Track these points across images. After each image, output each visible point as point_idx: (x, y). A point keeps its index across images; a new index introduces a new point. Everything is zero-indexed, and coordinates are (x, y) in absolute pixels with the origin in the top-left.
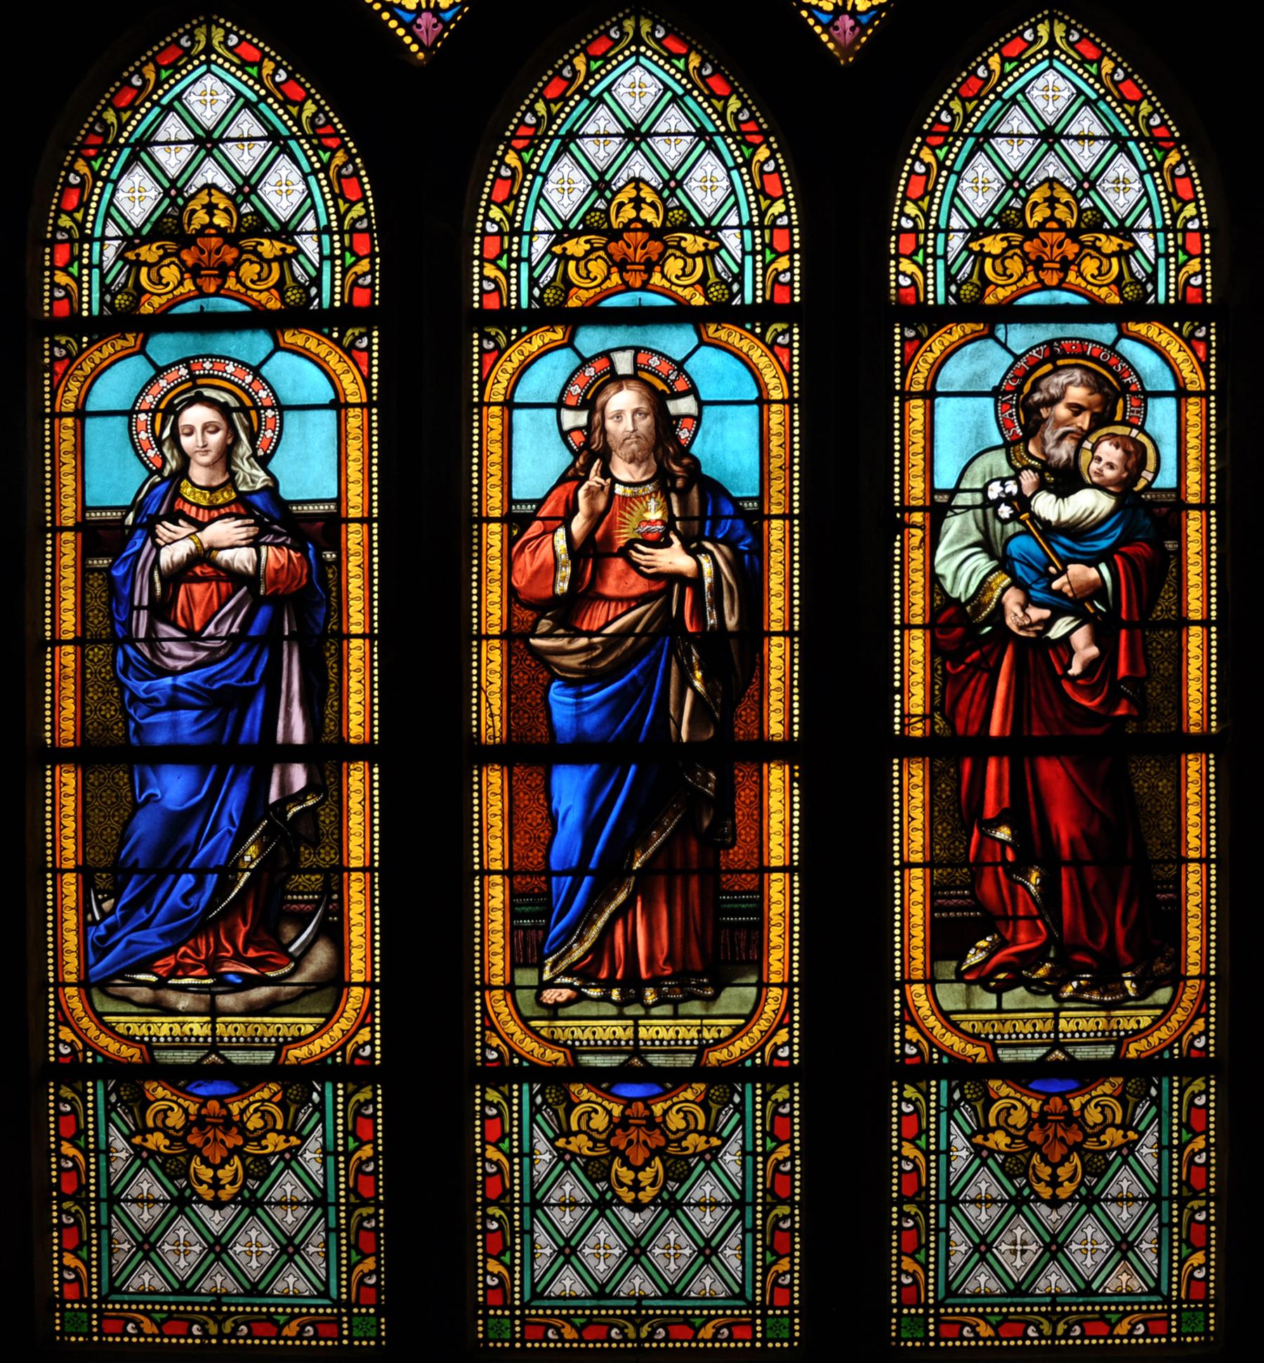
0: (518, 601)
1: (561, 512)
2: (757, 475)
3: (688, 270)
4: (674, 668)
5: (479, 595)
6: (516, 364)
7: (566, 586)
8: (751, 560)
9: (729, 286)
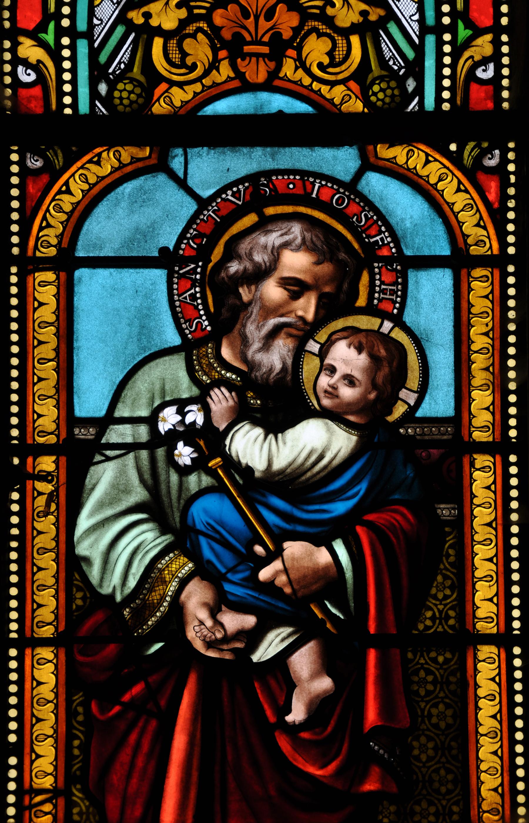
3: (339, 54)
9: (402, 82)
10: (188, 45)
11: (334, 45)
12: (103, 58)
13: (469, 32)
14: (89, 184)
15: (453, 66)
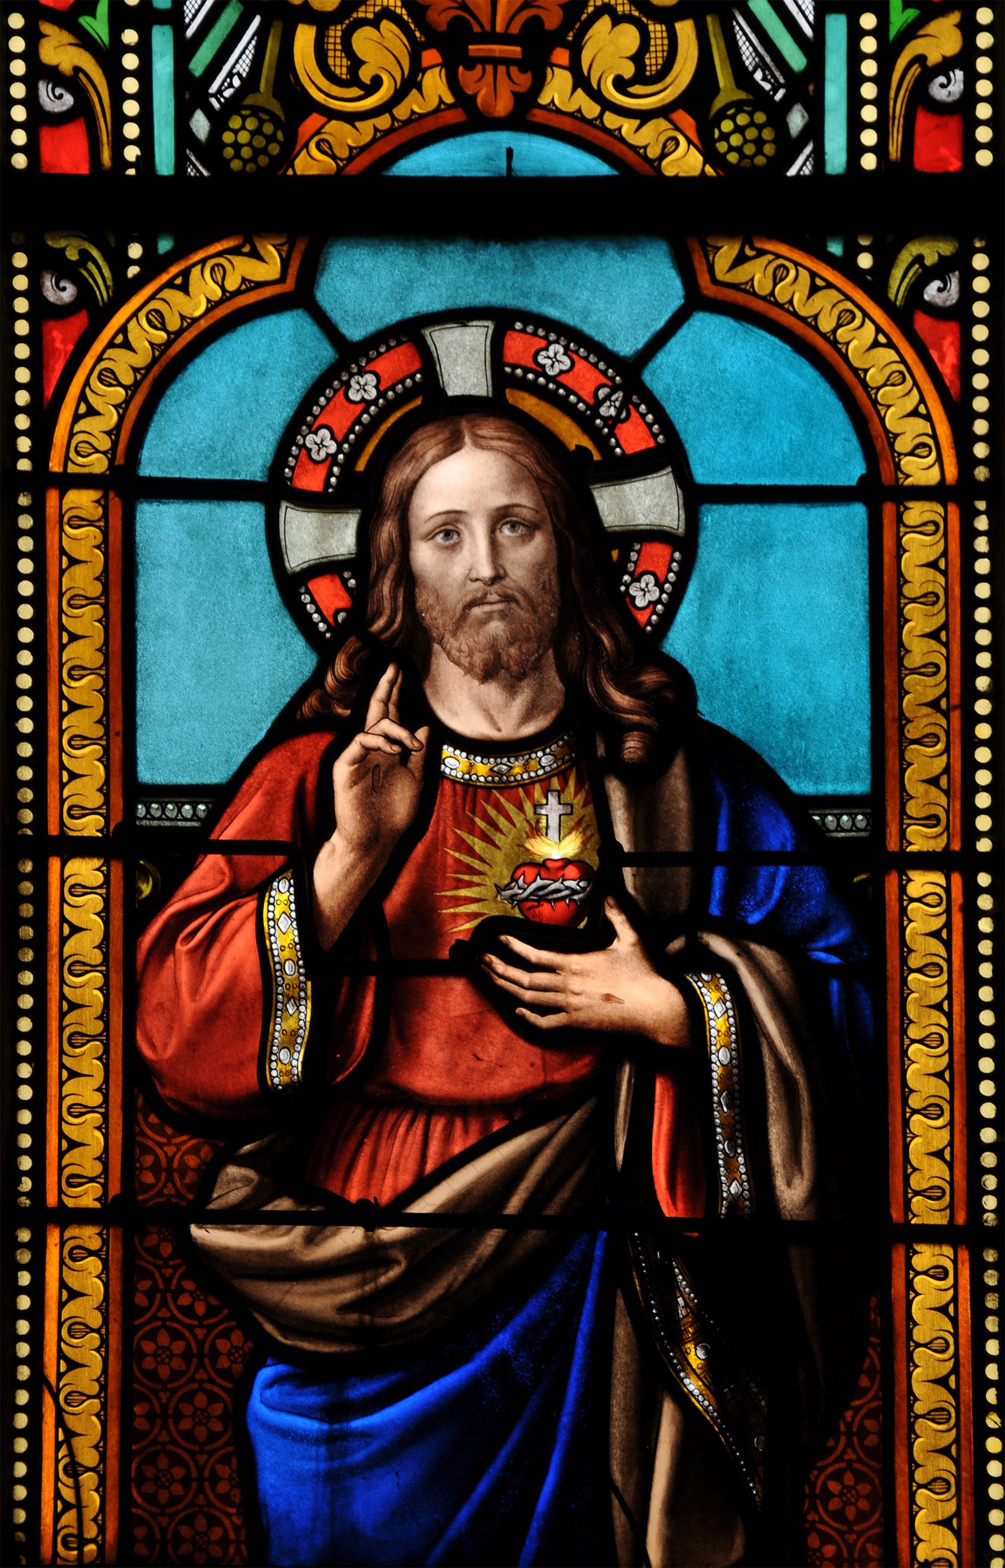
0: (156, 1104)
1: (281, 828)
2: (863, 728)
3: (653, 61)
4: (622, 1332)
5: (38, 1081)
6: (142, 357)
7: (297, 1060)
8: (848, 993)
9: (778, 115)
10: (363, 41)
11: (645, 37)
12: (198, 65)
13: (912, 13)
14: (168, 333)
15: (882, 80)
